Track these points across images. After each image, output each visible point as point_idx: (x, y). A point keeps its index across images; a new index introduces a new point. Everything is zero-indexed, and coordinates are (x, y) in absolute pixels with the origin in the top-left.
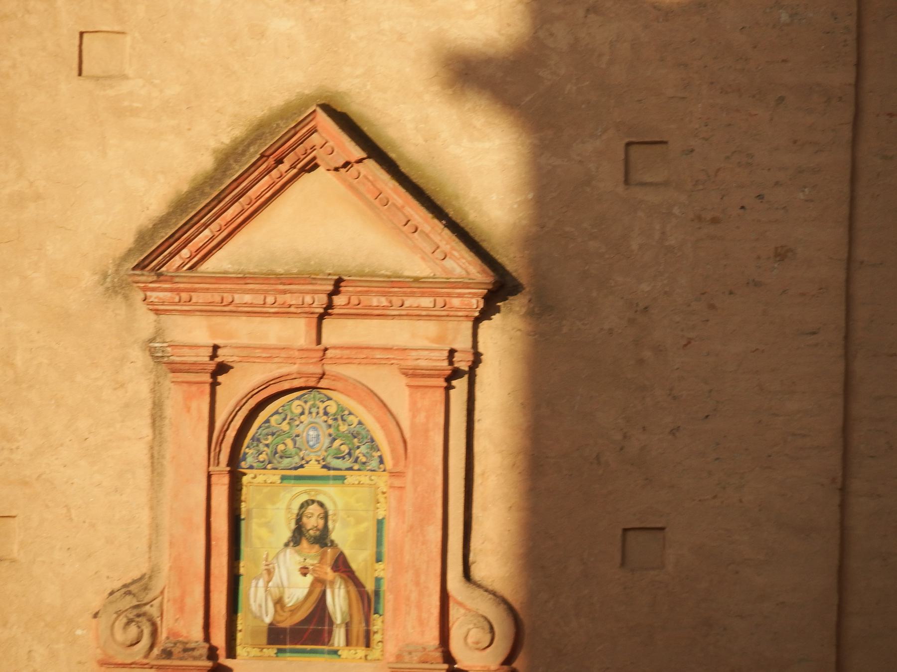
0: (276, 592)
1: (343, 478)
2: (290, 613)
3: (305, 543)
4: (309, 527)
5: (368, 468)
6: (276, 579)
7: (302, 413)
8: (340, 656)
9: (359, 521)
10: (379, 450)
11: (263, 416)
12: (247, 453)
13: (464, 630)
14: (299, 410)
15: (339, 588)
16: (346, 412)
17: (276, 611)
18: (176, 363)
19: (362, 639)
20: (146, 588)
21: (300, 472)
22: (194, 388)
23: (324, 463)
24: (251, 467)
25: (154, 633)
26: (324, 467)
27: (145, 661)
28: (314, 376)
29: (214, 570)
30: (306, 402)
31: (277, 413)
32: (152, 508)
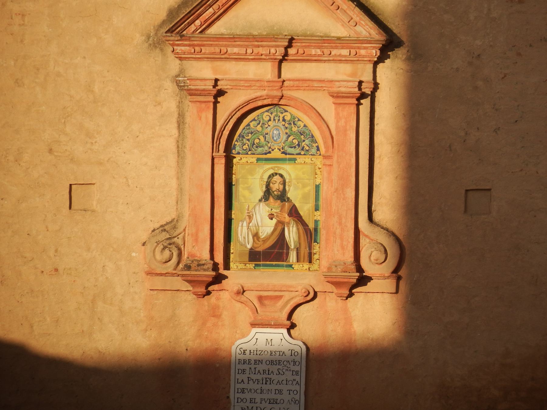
0: (254, 229)
3: (271, 199)
4: (274, 190)
5: (310, 153)
7: (270, 120)
9: (304, 186)
10: (316, 142)
12: (236, 145)
13: (370, 252)
14: (268, 118)
15: (293, 227)
16: (297, 119)
17: (254, 241)
19: (307, 258)
20: (175, 228)
21: (268, 156)
22: (203, 105)
24: (239, 153)
25: (180, 255)
26: (283, 153)
30: (271, 113)
31: (254, 120)
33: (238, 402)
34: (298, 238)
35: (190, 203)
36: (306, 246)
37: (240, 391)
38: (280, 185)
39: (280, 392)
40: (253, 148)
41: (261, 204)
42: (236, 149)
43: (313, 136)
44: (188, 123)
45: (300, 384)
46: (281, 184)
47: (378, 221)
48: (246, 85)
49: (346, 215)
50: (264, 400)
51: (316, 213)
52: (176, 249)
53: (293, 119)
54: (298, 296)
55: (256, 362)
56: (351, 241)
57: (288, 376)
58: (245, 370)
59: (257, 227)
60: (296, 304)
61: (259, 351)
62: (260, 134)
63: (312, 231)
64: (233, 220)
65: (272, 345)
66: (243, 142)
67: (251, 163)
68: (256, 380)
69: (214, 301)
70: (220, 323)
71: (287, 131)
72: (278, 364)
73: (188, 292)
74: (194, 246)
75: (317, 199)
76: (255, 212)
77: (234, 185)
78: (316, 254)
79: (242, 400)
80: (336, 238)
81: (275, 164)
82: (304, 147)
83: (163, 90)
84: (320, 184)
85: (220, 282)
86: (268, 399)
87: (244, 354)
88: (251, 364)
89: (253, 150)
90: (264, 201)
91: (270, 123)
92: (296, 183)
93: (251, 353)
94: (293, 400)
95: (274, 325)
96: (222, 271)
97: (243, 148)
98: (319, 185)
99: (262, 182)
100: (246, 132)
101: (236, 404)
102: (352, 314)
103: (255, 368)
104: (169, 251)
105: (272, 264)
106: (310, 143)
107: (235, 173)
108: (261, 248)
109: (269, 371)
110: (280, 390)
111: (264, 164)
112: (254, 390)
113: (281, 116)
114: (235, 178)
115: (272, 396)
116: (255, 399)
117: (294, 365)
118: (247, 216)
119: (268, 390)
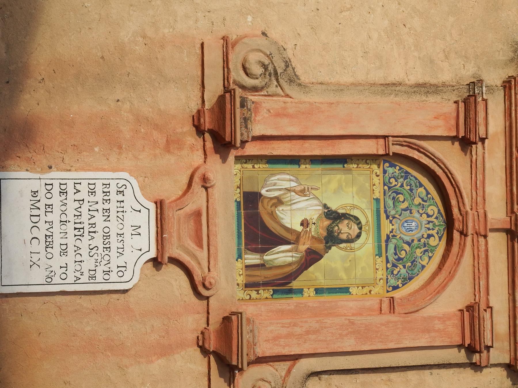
0: (286, 198)
1: (380, 255)
2: (270, 212)
3: (327, 223)
4: (340, 225)
5: (389, 276)
6: (297, 198)
7: (429, 216)
8: (237, 260)
9: (347, 270)
10: (403, 285)
11: (425, 181)
12: (395, 168)
13: (270, 379)
15: (292, 256)
16: (430, 255)
17: (271, 199)
18: (475, 107)
20: (291, 81)
21: (383, 216)
22: (453, 122)
23: (390, 236)
24: (385, 172)
25: (255, 89)
26: (388, 236)
27: (231, 82)
28: (465, 227)
29: (308, 144)
30: (437, 218)
31: (428, 193)
32: (352, 84)
33: (46, 184)
34: (278, 265)
35: (326, 105)
36: (267, 277)
37: (63, 187)
38: (346, 235)
39: (64, 252)
40: (392, 193)
41: (320, 208)
42: (390, 168)
43: (411, 279)
44: (427, 99)
45: (76, 282)
46: (348, 236)
47: (306, 385)
48: (478, 183)
49: (321, 341)
50: (51, 226)
51: (312, 289)
52: (263, 83)
53: (431, 249)
54: (203, 272)
55: (106, 212)
56: (286, 350)
57: (89, 264)
58: (94, 194)
59: (290, 203)
60: (191, 270)
61: (123, 216)
62: (411, 203)
63: (287, 286)
64: (297, 166)
65: (132, 235)
66: (399, 177)
67: (373, 190)
68: (81, 212)
69: (188, 142)
70: (158, 151)
71: (416, 242)
72: (105, 246)
73: (200, 102)
74: (270, 112)
75: (332, 291)
76: (309, 199)
77: (344, 167)
78: (258, 293)
79: (49, 191)
80: (288, 327)
81: (373, 227)
82: (397, 268)
83: (463, 63)
84: (350, 294)
85: (217, 151)
86: (52, 233)
87: (118, 191)
88: (103, 203)
89: (390, 193)
90: (324, 212)
91: (425, 216)
92: (350, 259)
93: (119, 203)
94: (53, 274)
95: (162, 237)
96: (233, 154)
97: (392, 178)
98: (349, 292)
99: (348, 208)
100: (412, 182)
101: (43, 182)
102: (177, 356)
103: (98, 210)
104: (261, 74)
105: (241, 229)
106: (402, 276)
107: (360, 168)
108: (263, 210)
109: (95, 232)
110: (66, 251)
111: (372, 210)
112: (65, 211)
113: (434, 232)
114: (353, 168)
115: (57, 240)
116: (52, 212)
117: (104, 272)
118: (305, 187)
119: (67, 233)
